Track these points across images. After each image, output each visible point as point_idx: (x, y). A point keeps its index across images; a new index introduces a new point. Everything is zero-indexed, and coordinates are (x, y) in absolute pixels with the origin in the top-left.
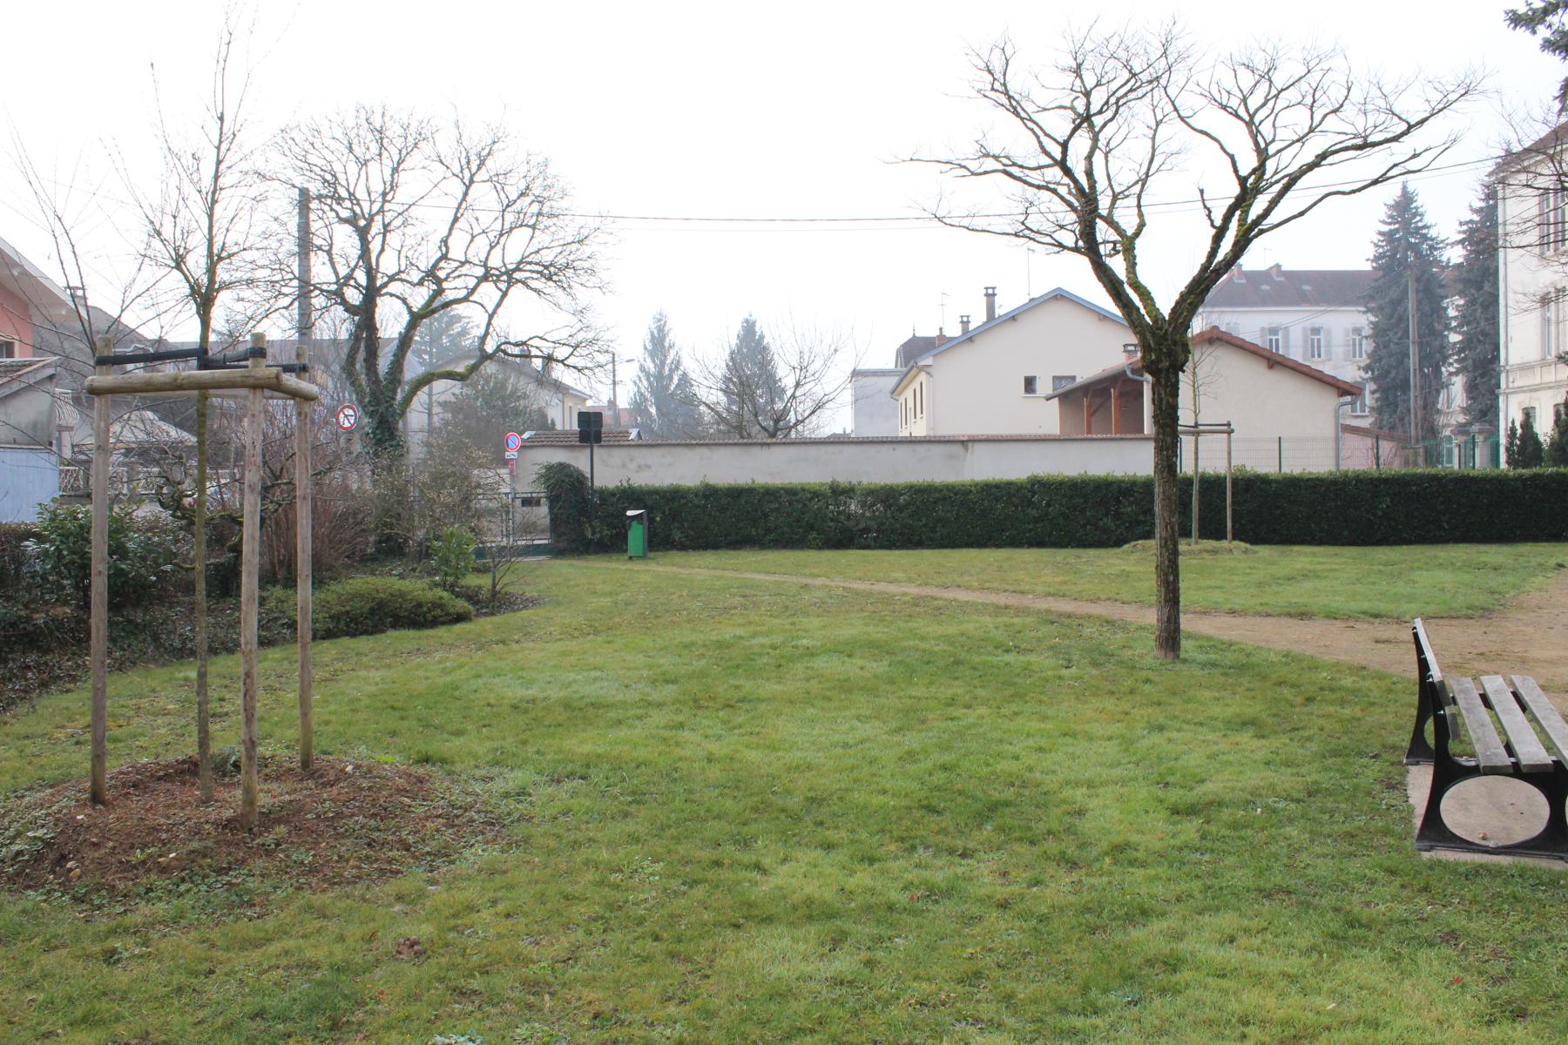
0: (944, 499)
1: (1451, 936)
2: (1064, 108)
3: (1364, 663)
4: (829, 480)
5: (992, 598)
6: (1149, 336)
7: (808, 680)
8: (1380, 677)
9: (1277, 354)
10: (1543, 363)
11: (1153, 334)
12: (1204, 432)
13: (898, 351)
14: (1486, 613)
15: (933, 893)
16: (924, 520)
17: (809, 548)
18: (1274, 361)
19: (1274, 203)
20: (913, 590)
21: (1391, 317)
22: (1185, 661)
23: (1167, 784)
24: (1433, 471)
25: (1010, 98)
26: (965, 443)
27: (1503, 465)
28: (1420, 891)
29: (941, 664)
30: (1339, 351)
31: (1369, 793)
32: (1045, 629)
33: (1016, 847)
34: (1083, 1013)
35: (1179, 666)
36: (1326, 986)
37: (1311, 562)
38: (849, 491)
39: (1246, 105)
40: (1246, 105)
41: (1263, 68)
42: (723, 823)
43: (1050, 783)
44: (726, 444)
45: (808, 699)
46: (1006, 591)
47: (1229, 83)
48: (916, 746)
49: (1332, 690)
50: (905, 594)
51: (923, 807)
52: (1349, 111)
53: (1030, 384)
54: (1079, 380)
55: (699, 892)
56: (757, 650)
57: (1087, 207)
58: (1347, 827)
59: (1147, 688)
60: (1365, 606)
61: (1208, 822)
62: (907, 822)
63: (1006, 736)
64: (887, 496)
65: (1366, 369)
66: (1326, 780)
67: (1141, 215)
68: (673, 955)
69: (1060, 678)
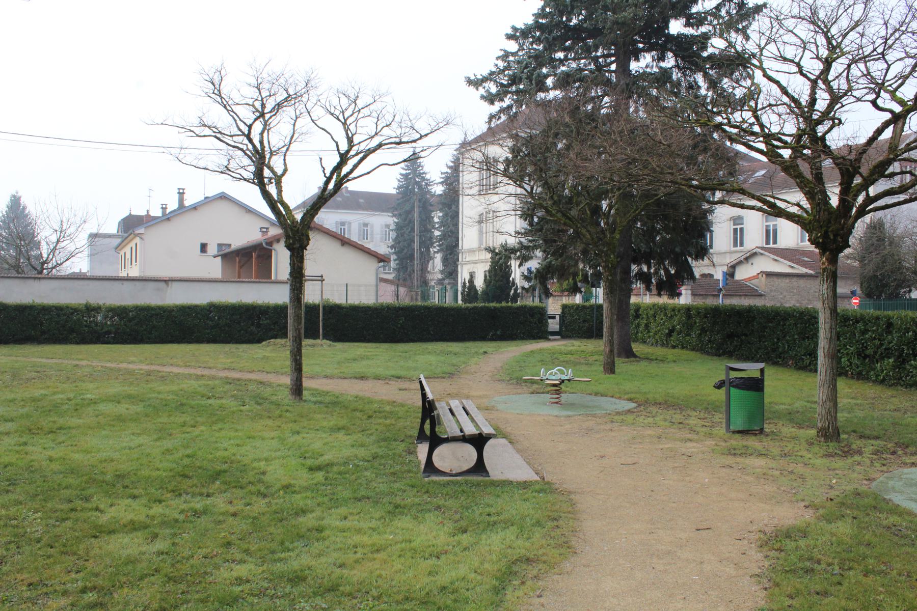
0: (157, 315)
1: (438, 508)
2: (249, 105)
3: (395, 400)
4: (84, 302)
5: (192, 371)
6: (289, 230)
7: (97, 416)
8: (403, 406)
9: (344, 237)
10: (479, 249)
11: (292, 230)
12: (309, 280)
13: (119, 223)
14: (451, 375)
15: (196, 513)
16: (144, 327)
17: (71, 343)
18: (345, 242)
19: (355, 166)
20: (145, 367)
21: (405, 220)
22: (305, 401)
23: (305, 458)
24: (426, 304)
25: (222, 98)
26: (166, 281)
27: (460, 302)
28: (425, 493)
29: (174, 405)
30: (378, 237)
31: (400, 456)
32: (227, 387)
33: (234, 490)
34: (283, 551)
35: (302, 403)
36: (388, 530)
37: (365, 351)
38: (97, 309)
39: (343, 115)
40: (343, 115)
41: (353, 97)
42: (70, 491)
43: (246, 460)
44: (9, 277)
45: (100, 426)
46: (200, 367)
47: (335, 102)
48: (170, 446)
49: (380, 412)
50: (141, 369)
51: (182, 475)
52: (394, 125)
53: (204, 247)
54: (233, 247)
55: (69, 523)
56: (59, 401)
57: (260, 158)
58: (392, 470)
59: (288, 414)
60: (393, 372)
61: (328, 472)
62: (173, 483)
63: (218, 440)
64: (121, 312)
65: (392, 247)
66: (380, 452)
67: (285, 164)
68: (63, 553)
69: (241, 411)
